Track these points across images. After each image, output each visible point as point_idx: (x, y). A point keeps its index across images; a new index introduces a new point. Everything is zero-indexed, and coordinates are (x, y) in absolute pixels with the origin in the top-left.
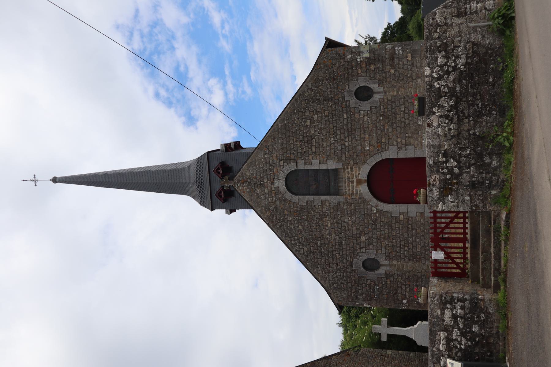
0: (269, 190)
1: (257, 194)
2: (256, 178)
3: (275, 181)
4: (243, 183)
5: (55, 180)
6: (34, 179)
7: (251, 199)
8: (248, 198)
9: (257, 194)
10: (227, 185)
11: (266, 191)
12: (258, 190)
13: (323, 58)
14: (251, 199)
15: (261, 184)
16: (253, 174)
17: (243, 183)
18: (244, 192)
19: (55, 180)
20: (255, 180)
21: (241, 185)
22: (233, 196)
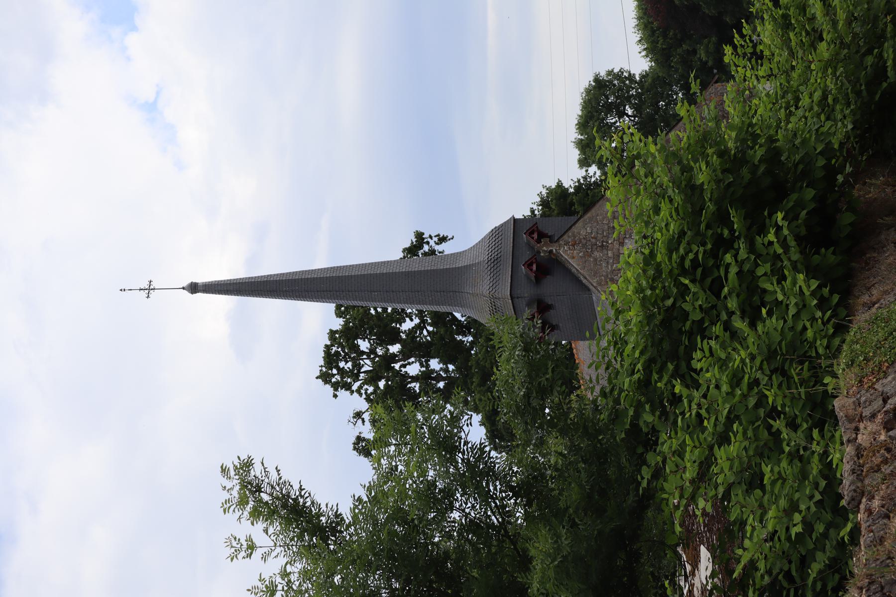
0: (615, 254)
1: (595, 260)
2: (595, 238)
3: (626, 241)
4: (573, 245)
5: (194, 288)
6: (147, 291)
7: (584, 267)
8: (578, 265)
9: (595, 260)
10: (546, 249)
11: (610, 255)
12: (597, 254)
13: (710, 94)
14: (584, 267)
15: (603, 245)
16: (592, 232)
17: (573, 245)
18: (573, 258)
19: (194, 288)
20: (594, 240)
21: (569, 248)
22: (548, 275)
